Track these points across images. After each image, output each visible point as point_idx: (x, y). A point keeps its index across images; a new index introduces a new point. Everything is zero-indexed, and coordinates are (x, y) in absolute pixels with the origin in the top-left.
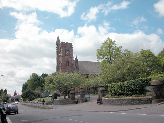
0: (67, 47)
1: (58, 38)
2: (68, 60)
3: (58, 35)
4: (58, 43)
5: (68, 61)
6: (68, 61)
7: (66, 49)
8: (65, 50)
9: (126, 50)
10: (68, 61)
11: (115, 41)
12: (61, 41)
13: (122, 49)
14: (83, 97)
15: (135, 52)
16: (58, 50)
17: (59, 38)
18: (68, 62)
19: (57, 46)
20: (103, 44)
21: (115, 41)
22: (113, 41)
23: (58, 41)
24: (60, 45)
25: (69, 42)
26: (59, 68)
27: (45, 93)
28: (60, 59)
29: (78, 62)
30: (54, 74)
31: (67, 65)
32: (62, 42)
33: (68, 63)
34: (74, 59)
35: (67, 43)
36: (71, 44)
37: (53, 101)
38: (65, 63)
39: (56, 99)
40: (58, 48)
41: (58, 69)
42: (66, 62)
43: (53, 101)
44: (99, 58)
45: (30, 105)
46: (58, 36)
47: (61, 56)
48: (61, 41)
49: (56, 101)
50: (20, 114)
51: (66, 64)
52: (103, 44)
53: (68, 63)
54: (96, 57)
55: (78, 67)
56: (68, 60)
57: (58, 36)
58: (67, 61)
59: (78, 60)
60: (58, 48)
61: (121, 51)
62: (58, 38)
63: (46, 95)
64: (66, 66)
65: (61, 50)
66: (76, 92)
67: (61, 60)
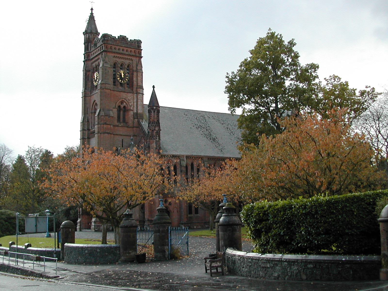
0: (117, 53)
1: (92, 18)
2: (122, 102)
3: (92, 9)
4: (92, 37)
5: (122, 106)
6: (124, 107)
7: (120, 61)
8: (115, 64)
9: (335, 77)
10: (122, 106)
11: (292, 43)
12: (102, 29)
13: (319, 72)
14: (162, 242)
15: (363, 88)
16: (90, 63)
17: (96, 19)
18: (123, 110)
19: (86, 49)
20: (252, 52)
21: (292, 43)
22: (286, 43)
23: (91, 32)
24: (95, 45)
25: (131, 37)
26: (89, 130)
27: (34, 219)
28: (96, 97)
29: (158, 112)
30: (70, 154)
31: (119, 120)
32: (105, 36)
33: (122, 112)
34: (146, 100)
35: (123, 39)
36: (136, 45)
37: (60, 249)
38: (114, 113)
39: (74, 243)
40: (88, 56)
41: (87, 133)
42: (115, 110)
43: (60, 249)
44: (234, 103)
45: (97, 55)
46: (92, 14)
47: (99, 87)
48: (102, 29)
49: (71, 252)
50: (143, 111)
51: (116, 116)
52: (252, 52)
53: (122, 112)
54: (226, 98)
55: (160, 130)
56: (122, 102)
57: (92, 14)
58: (118, 104)
59: (161, 104)
60: (88, 56)
61: (317, 81)
62: (92, 18)
63: (36, 226)
64: (116, 123)
65: (101, 66)
66: (146, 217)
67: (99, 103)
